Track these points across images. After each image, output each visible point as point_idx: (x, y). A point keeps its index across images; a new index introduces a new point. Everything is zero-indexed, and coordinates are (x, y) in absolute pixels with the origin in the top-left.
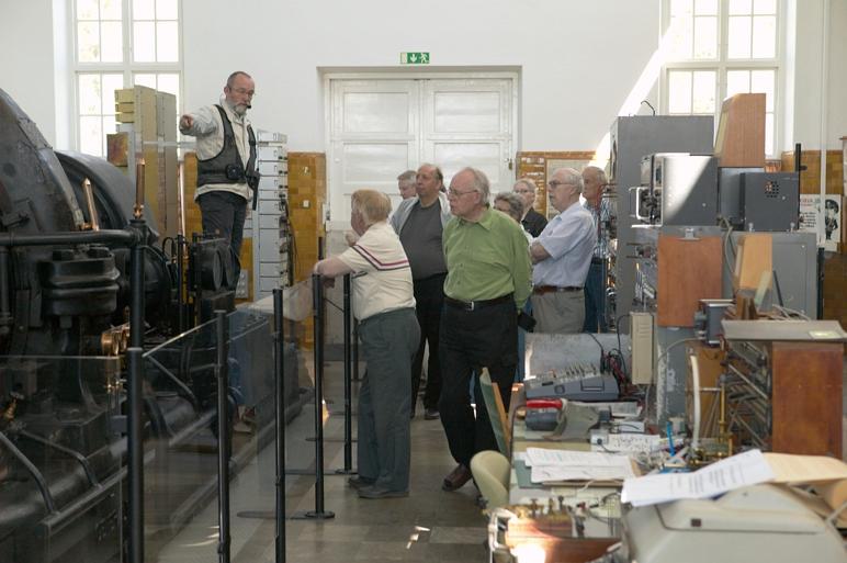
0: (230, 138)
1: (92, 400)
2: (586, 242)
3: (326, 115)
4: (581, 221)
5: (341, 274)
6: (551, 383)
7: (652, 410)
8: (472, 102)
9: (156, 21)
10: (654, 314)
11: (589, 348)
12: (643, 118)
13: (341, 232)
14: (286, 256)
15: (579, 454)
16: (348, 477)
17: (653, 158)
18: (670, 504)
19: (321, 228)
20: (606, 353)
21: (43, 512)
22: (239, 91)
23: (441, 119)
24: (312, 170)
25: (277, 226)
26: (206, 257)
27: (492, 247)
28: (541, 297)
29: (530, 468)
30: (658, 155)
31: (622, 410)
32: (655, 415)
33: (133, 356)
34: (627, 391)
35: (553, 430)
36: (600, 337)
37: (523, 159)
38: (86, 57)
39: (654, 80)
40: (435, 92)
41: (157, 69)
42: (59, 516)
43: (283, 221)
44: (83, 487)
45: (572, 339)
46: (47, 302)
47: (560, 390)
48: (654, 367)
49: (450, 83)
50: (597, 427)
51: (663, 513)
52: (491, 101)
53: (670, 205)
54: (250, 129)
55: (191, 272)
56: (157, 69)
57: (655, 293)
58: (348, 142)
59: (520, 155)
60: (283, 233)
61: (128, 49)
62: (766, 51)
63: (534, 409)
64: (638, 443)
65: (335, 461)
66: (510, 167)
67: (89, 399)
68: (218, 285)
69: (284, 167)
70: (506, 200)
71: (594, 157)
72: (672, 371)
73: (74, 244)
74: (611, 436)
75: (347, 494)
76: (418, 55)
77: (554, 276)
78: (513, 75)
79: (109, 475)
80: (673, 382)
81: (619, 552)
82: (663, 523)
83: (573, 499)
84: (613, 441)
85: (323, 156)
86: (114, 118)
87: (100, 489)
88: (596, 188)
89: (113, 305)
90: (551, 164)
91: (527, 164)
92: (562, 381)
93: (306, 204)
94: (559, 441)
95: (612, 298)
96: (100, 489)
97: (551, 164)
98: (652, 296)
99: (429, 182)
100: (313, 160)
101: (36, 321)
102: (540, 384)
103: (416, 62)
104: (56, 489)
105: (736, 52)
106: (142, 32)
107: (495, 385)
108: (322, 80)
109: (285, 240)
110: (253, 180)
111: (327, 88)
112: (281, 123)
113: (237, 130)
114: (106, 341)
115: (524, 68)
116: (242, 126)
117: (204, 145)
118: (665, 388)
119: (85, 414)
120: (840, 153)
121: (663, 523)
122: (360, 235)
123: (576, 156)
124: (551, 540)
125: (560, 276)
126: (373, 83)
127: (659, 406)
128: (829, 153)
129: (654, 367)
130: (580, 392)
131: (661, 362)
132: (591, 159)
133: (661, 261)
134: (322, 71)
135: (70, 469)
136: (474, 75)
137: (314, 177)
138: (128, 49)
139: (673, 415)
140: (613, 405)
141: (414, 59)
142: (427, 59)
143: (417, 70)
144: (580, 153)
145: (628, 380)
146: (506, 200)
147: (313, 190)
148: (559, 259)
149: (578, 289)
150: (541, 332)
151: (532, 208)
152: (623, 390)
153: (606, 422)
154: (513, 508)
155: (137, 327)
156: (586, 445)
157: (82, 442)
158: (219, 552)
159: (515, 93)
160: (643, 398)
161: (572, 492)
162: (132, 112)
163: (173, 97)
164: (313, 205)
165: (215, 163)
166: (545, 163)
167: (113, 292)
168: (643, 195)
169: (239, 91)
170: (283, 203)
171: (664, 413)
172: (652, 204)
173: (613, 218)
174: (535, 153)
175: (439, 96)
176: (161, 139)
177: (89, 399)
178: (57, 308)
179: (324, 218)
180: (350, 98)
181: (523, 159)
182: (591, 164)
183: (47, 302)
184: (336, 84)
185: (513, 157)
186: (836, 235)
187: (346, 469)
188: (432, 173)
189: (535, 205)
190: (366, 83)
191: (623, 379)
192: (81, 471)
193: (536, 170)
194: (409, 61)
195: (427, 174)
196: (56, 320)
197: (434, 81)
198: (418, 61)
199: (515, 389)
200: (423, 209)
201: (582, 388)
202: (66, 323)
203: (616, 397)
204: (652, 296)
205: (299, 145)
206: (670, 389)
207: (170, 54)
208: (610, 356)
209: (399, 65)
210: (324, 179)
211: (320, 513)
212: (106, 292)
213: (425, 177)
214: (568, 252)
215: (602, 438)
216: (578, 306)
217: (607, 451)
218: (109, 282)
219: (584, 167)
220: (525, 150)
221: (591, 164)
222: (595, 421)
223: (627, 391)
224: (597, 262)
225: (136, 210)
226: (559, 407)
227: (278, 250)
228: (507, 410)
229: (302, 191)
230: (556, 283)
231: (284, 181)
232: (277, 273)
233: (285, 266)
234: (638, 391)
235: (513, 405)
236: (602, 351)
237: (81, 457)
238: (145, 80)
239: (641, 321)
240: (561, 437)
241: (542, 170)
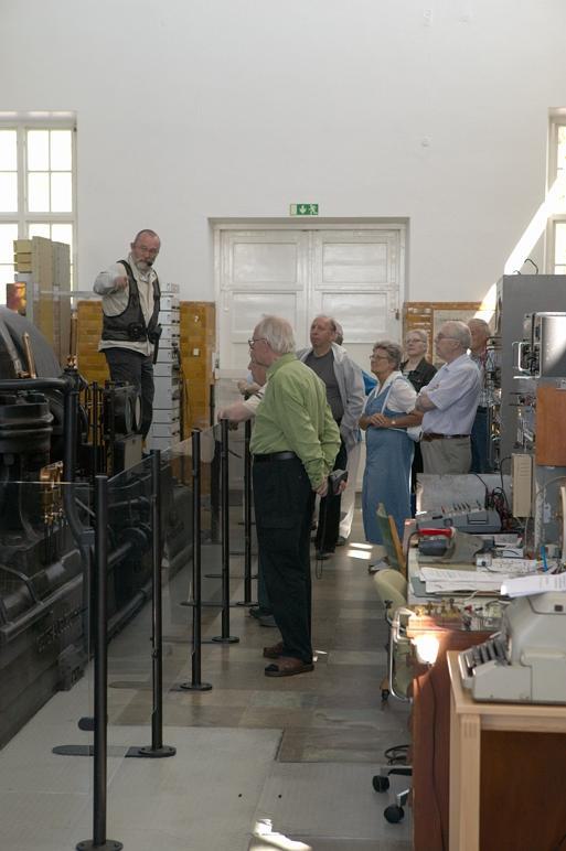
0: (134, 297)
1: (31, 529)
2: (473, 393)
3: (216, 263)
4: (469, 373)
5: (242, 421)
6: (441, 517)
7: (530, 539)
8: (359, 252)
9: (50, 172)
10: (534, 456)
11: (475, 487)
12: (527, 277)
13: (230, 380)
14: (177, 403)
15: (470, 573)
16: (248, 609)
17: (534, 316)
18: (538, 596)
19: (211, 376)
20: (490, 491)
22: (145, 250)
23: (329, 271)
24: (202, 319)
25: (169, 373)
26: (119, 402)
27: (94, 507)
28: (430, 444)
29: (424, 582)
30: (538, 314)
31: (504, 540)
32: (533, 542)
33: (100, 482)
34: (509, 524)
35: (440, 553)
36: (486, 477)
37: (410, 309)
39: (552, 189)
40: (324, 243)
41: (50, 219)
42: (13, 625)
43: (176, 369)
44: (27, 604)
45: (459, 479)
47: (449, 522)
48: (533, 500)
49: (339, 234)
50: (481, 552)
51: (534, 604)
52: (379, 251)
53: (547, 359)
54: (156, 284)
56: (50, 219)
57: (534, 437)
58: (237, 292)
59: (407, 305)
60: (175, 381)
61: (22, 199)
63: (426, 536)
64: (518, 565)
65: (237, 595)
66: (397, 317)
67: (29, 529)
68: (129, 429)
69: (176, 316)
70: (385, 348)
71: (481, 308)
72: (549, 505)
73: (15, 390)
74: (494, 560)
75: (247, 623)
76: (307, 206)
77: (441, 425)
78: (402, 227)
79: (50, 592)
80: (550, 515)
81: (499, 638)
82: (532, 608)
83: (461, 603)
84: (496, 563)
85: (213, 305)
86: (13, 267)
87: (42, 605)
88: (479, 340)
89: (47, 444)
90: (438, 315)
91: (415, 315)
92: (450, 515)
93: (196, 352)
94: (448, 563)
95: (496, 443)
96: (42, 605)
97: (438, 315)
98: (531, 439)
99: (324, 332)
100: (204, 310)
102: (431, 519)
103: (306, 213)
106: (36, 184)
107: (390, 517)
108: (212, 231)
109: (177, 387)
110: (153, 334)
111: (217, 238)
112: (182, 274)
113: (142, 288)
115: (411, 220)
116: (147, 283)
117: (110, 303)
118: (542, 519)
121: (532, 608)
123: (462, 306)
124: (445, 633)
125: (447, 426)
126: (263, 234)
127: (537, 535)
129: (533, 500)
130: (466, 525)
131: (539, 497)
132: (478, 309)
133: (539, 409)
135: (17, 588)
136: (362, 226)
137: (204, 326)
139: (548, 543)
140: (496, 536)
141: (303, 210)
142: (317, 210)
143: (306, 221)
144: (466, 304)
145: (510, 516)
146: (385, 348)
147: (204, 339)
148: (446, 409)
149: (464, 436)
150: (429, 472)
151: (424, 359)
152: (505, 525)
153: (490, 549)
154: (412, 608)
155: (69, 467)
156: (473, 567)
157: (26, 564)
158: (153, 656)
159: (403, 244)
160: (523, 531)
161: (461, 600)
162: (29, 263)
163: (68, 246)
164: (203, 352)
165: (119, 321)
166: (431, 314)
167: (48, 432)
168: (525, 349)
169: (145, 250)
170: (176, 351)
171: (541, 541)
172: (532, 358)
173: (498, 369)
174: (421, 304)
175: (328, 248)
176: (56, 289)
177: (29, 529)
179: (214, 366)
180: (240, 248)
181: (410, 309)
182: (478, 315)
184: (226, 235)
185: (400, 307)
187: (246, 601)
188: (326, 324)
189: (427, 355)
190: (254, 234)
191: (505, 515)
192: (25, 590)
193: (423, 320)
194: (299, 213)
195: (323, 325)
197: (323, 233)
198: (307, 213)
199: (407, 523)
200: (318, 359)
201: (468, 521)
203: (499, 530)
204: (531, 439)
205: (192, 293)
206: (547, 521)
207: (64, 205)
208: (494, 494)
209: (288, 215)
210: (214, 328)
211: (226, 638)
212: (44, 432)
213: (320, 327)
214: (455, 403)
215: (486, 561)
216: (464, 453)
217: (490, 571)
218: (45, 425)
219: (469, 319)
220: (412, 300)
221: (478, 315)
222: (480, 548)
223: (509, 524)
224: (481, 411)
225: (69, 360)
226: (448, 534)
227: (170, 397)
228: (401, 540)
229: (191, 340)
230: (443, 432)
231: (177, 330)
232: (169, 420)
233: (177, 413)
234: (518, 524)
235: (407, 535)
236: (487, 491)
237: (26, 578)
238: (37, 230)
239: (521, 462)
240: (451, 561)
241: (429, 320)
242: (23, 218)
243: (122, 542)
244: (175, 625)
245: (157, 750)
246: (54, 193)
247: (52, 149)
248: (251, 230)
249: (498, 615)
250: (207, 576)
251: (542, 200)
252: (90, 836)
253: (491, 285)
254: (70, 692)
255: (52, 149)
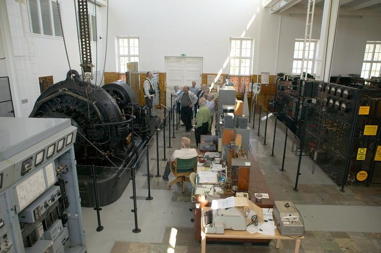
21: (119, 174)
24: (164, 76)
38: (121, 53)
41: (134, 56)
43: (158, 88)
55: (141, 114)
56: (134, 56)
61: (129, 52)
62: (248, 55)
101: (115, 135)
104: (120, 168)
106: (132, 49)
114: (127, 139)
119: (124, 152)
134: (165, 57)
138: (129, 52)
164: (164, 82)
177: (125, 149)
178: (119, 134)
196: (119, 136)
202: (120, 136)
207: (137, 53)
217: (213, 171)
242: (129, 56)
243: (145, 139)
244: (161, 144)
245: (149, 198)
246: (135, 51)
250: (152, 159)
252: (135, 228)
254: (185, 85)
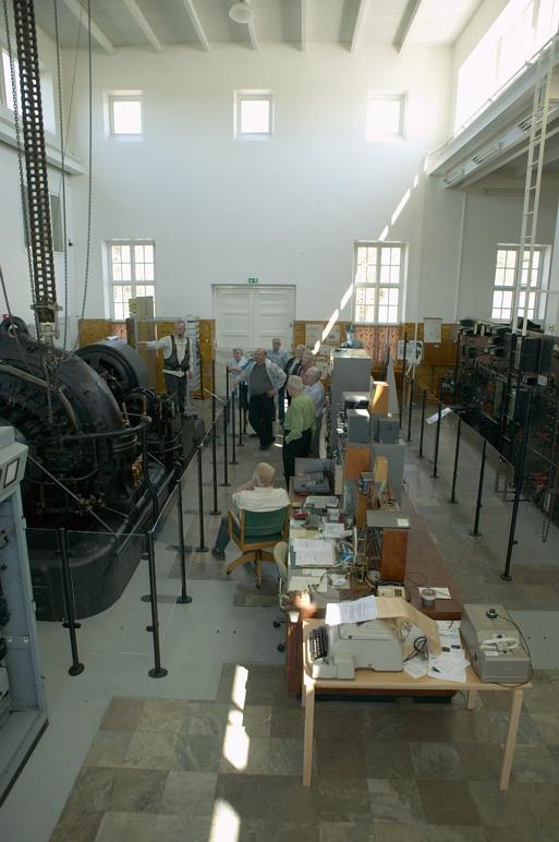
21: (116, 546)
46: (111, 454)
61: (133, 275)
62: (396, 280)
105: (384, 280)
114: (134, 468)
120: (423, 324)
122: (224, 559)
128: (419, 324)
164: (210, 339)
178: (115, 457)
183: (111, 454)
186: (420, 357)
196: (115, 461)
243: (172, 468)
247: (145, 254)
248: (23, 742)
249: (348, 411)
251: (246, 687)
252: (153, 666)
253: (209, 813)
255: (145, 254)
